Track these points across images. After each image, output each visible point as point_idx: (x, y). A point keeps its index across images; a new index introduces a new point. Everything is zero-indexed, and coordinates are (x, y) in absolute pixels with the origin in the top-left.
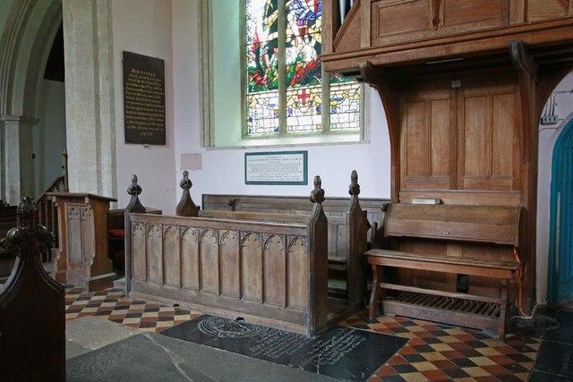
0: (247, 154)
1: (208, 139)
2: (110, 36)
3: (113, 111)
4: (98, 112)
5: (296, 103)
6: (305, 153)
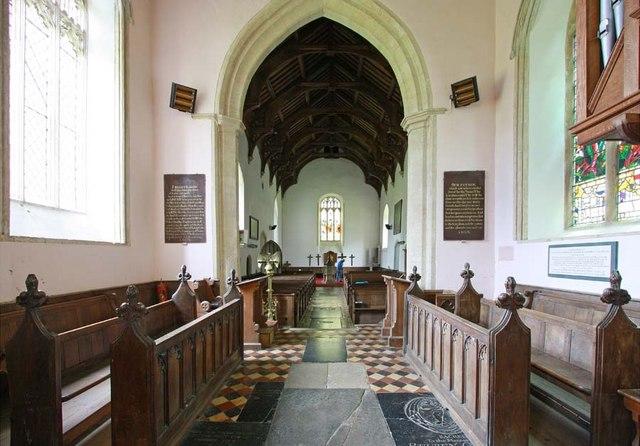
0: (550, 247)
1: (521, 232)
2: (434, 164)
3: (434, 218)
4: (424, 219)
5: (631, 186)
6: (615, 245)
